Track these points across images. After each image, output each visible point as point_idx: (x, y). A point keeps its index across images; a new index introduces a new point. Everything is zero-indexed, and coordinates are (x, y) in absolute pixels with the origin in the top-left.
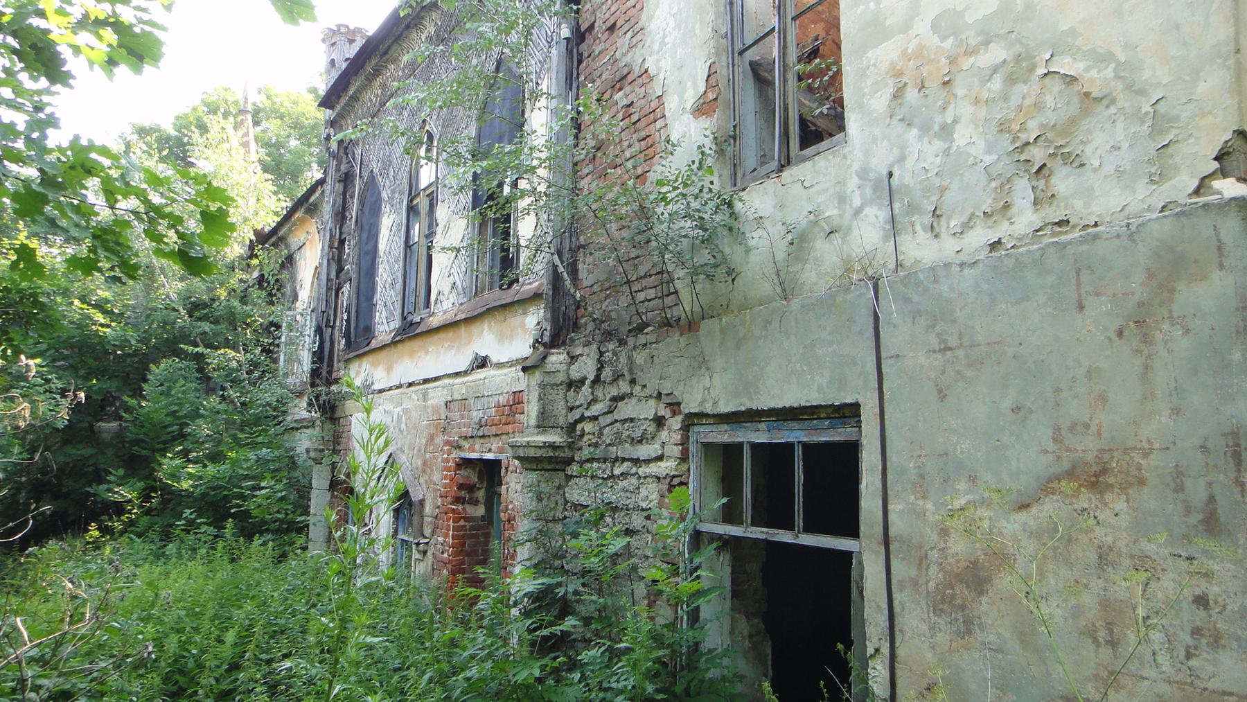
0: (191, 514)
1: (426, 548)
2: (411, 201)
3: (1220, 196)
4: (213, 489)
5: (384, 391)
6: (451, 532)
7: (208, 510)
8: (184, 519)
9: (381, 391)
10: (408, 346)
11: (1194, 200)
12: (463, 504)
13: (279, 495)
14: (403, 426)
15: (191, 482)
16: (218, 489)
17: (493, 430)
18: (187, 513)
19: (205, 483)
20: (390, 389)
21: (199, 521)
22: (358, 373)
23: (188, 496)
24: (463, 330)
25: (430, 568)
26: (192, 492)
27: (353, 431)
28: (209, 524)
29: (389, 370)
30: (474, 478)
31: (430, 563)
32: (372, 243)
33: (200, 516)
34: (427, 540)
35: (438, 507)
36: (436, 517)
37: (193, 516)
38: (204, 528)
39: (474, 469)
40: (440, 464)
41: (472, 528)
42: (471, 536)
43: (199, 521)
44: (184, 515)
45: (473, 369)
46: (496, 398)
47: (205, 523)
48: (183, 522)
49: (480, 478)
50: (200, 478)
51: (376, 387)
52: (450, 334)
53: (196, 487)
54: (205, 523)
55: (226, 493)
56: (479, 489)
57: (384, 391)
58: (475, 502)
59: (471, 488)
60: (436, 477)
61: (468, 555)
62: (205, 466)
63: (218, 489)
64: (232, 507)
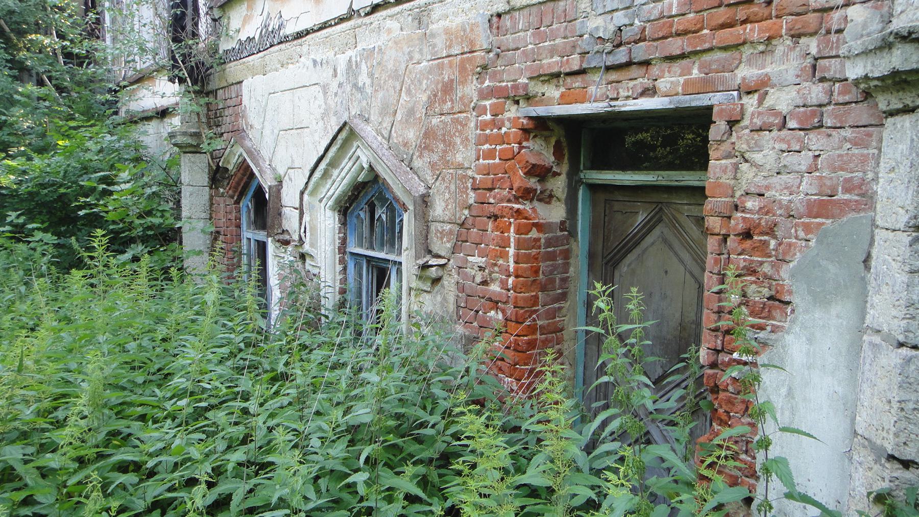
0: (18, 217)
1: (440, 273)
3: (11, 415)
4: (43, 186)
5: (308, 32)
6: (511, 251)
7: (40, 213)
8: (11, 223)
9: (299, 35)
11: (352, 403)
12: (531, 200)
13: (148, 191)
14: (363, 79)
15: (12, 177)
16: (53, 185)
17: (676, 46)
18: (12, 216)
19: (31, 180)
21: (30, 226)
22: (246, 20)
23: (12, 196)
25: (452, 307)
26: (16, 190)
27: (245, 101)
28: (45, 230)
30: (548, 158)
31: (451, 299)
33: (32, 220)
34: (443, 261)
35: (469, 207)
36: (462, 225)
37: (21, 220)
38: (39, 235)
39: (546, 139)
40: (472, 132)
41: (549, 243)
42: (551, 257)
43: (30, 226)
44: (9, 219)
47: (38, 229)
48: (8, 228)
49: (558, 152)
50: (24, 172)
51: (290, 29)
53: (20, 183)
54: (38, 229)
55: (62, 190)
56: (556, 174)
57: (308, 32)
58: (547, 198)
59: (540, 172)
60: (464, 155)
61: (543, 289)
62: (30, 159)
63: (53, 185)
64: (80, 208)
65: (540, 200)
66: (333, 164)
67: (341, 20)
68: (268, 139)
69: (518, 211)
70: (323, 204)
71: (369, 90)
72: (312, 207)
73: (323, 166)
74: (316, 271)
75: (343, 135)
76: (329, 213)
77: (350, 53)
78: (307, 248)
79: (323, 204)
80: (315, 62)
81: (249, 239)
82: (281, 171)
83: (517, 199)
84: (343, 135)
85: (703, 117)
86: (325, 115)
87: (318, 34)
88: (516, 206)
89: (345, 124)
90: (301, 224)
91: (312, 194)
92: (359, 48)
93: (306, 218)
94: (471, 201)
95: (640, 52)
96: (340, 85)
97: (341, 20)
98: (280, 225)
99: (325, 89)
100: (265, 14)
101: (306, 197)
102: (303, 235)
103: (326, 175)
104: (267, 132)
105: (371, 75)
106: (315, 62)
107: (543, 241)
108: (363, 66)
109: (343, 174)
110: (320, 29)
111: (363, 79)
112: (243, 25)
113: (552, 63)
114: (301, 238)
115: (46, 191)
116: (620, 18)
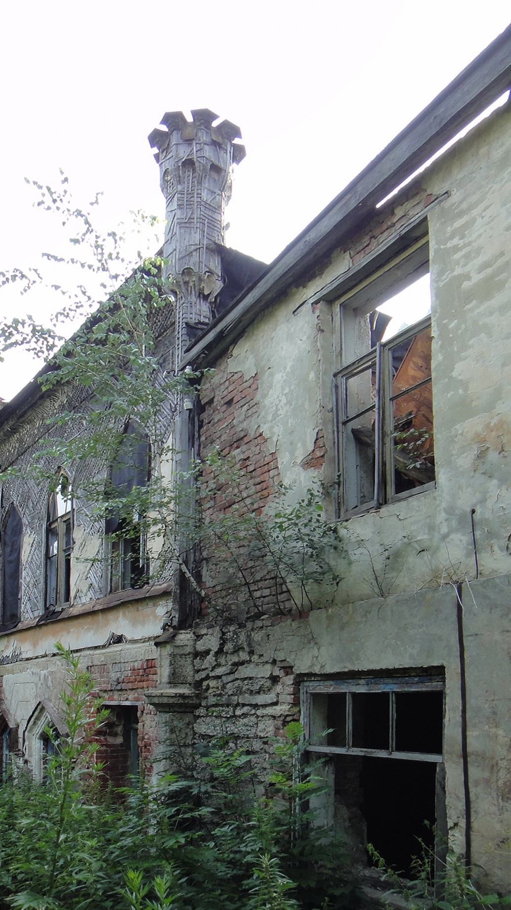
2: (50, 525)
9: (27, 659)
10: (51, 628)
20: (37, 658)
24: (100, 617)
27: (4, 686)
29: (35, 645)
32: (16, 555)
41: (112, 752)
45: (110, 644)
46: (132, 664)
51: (24, 656)
52: (89, 619)
56: (117, 725)
58: (115, 735)
65: (109, 735)
66: (38, 718)
67: (43, 657)
68: (13, 706)
69: (97, 739)
70: (34, 737)
71: (52, 688)
72: (29, 738)
73: (33, 719)
74: (31, 768)
75: (39, 707)
76: (38, 741)
77: (45, 671)
78: (26, 757)
79: (34, 737)
80: (33, 672)
81: (6, 755)
82: (19, 721)
83: (96, 735)
84: (39, 707)
85: (135, 708)
86: (36, 697)
87: (35, 660)
88: (96, 737)
89: (40, 702)
90: (23, 746)
91: (29, 732)
92: (49, 669)
93: (26, 743)
94: (84, 736)
95: (124, 686)
96: (42, 684)
97: (43, 657)
98: (18, 747)
99: (36, 684)
100: (15, 646)
101: (26, 733)
102: (24, 751)
103: (35, 723)
104: (13, 702)
105: (52, 682)
106: (33, 672)
107: (109, 751)
108: (50, 678)
109: (42, 723)
110: (36, 658)
111: (50, 683)
112: (5, 649)
113: (104, 687)
114: (23, 753)
115: (345, 875)
116: (119, 675)
